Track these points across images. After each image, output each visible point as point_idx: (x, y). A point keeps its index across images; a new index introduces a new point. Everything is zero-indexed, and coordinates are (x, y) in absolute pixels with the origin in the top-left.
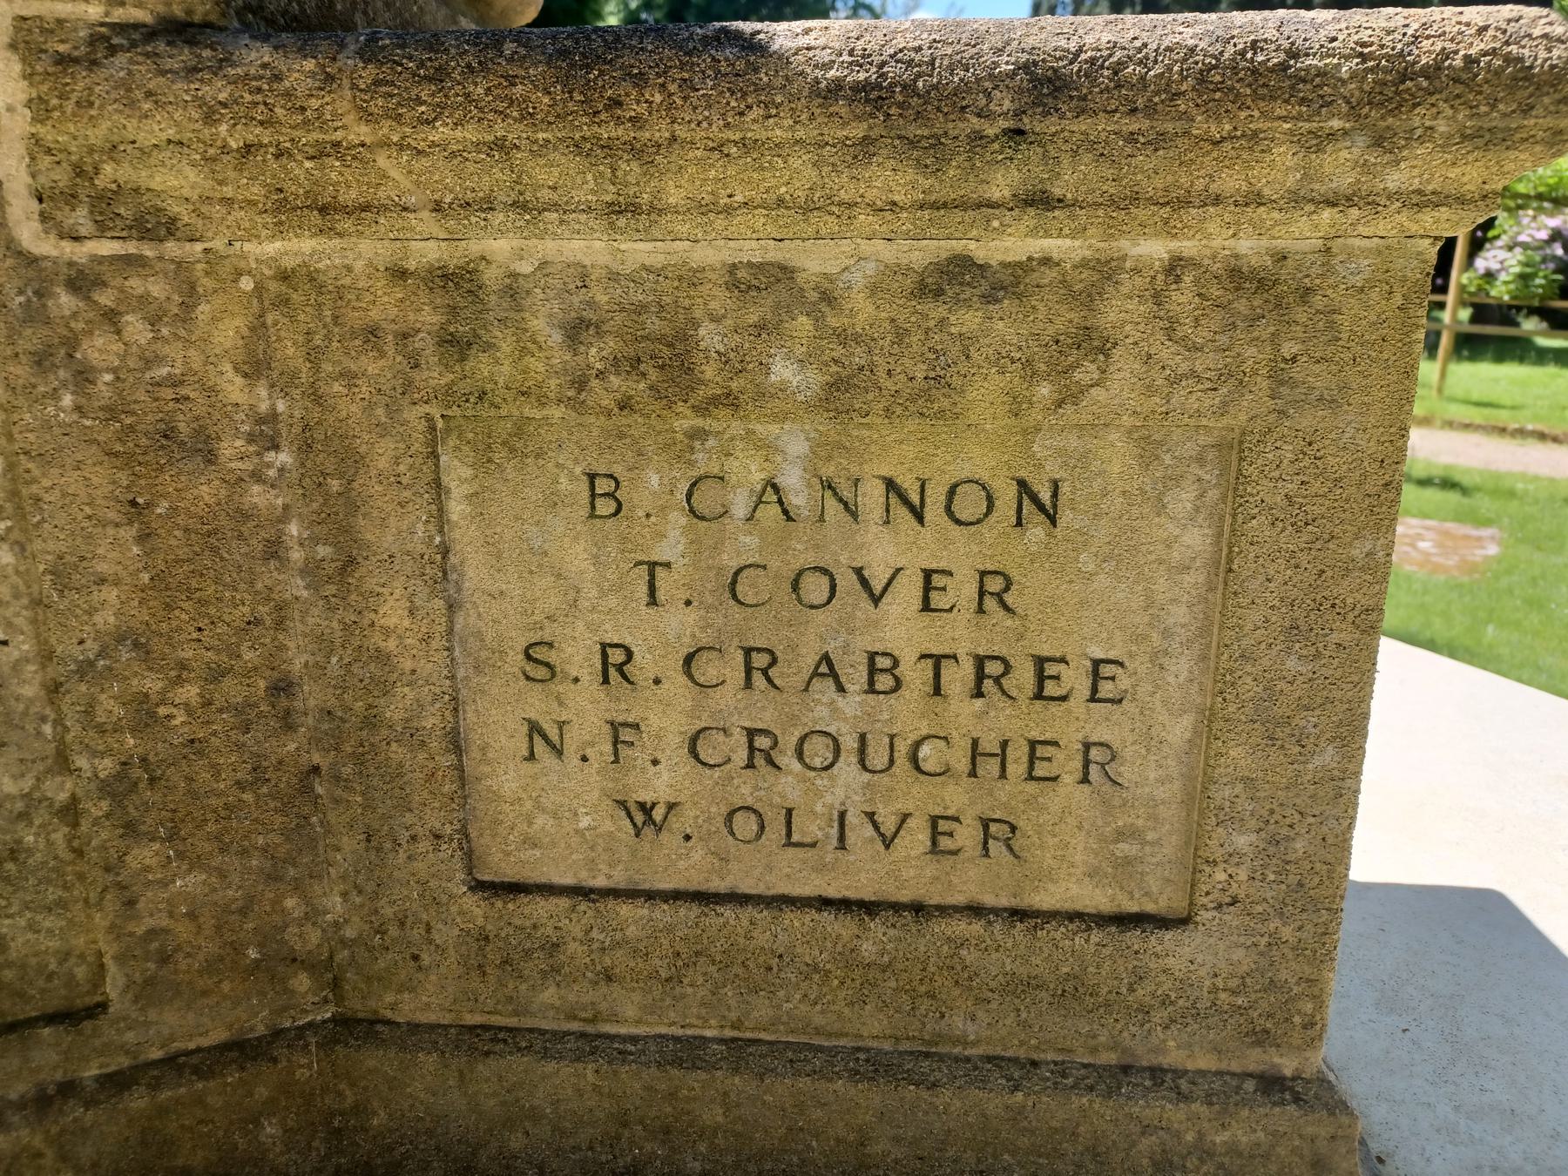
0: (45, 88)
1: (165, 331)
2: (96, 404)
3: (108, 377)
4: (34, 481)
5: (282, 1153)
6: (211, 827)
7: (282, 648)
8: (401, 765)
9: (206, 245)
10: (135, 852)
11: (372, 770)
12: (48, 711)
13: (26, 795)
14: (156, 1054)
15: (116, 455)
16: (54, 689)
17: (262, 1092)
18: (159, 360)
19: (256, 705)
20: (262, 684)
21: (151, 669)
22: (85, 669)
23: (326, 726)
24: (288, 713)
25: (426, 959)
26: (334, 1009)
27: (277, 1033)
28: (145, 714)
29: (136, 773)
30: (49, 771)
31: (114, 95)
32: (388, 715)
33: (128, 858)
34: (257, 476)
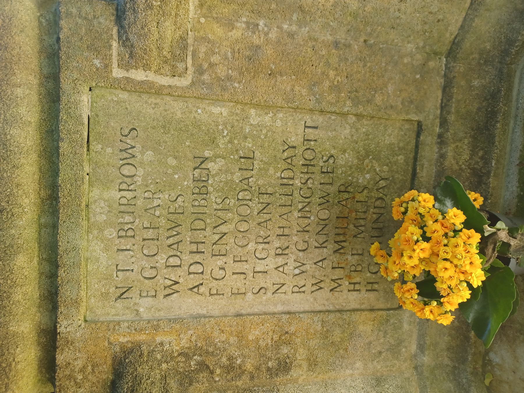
0: (140, 64)
1: (217, 50)
2: (238, 77)
3: (230, 71)
4: (260, 100)
5: (485, 80)
6: (375, 78)
7: (323, 41)
8: (373, 8)
9: (189, 30)
10: (377, 102)
11: (372, 20)
12: (328, 116)
13: (351, 127)
14: (439, 112)
15: (254, 76)
16: (322, 111)
17: (463, 83)
18: (226, 54)
19: (340, 55)
20: (334, 51)
21: (322, 83)
22: (318, 101)
23: (352, 34)
24: (344, 45)
25: (441, 17)
26: (443, 57)
27: (445, 75)
28: (336, 88)
29: (353, 95)
30: (345, 120)
31: (142, 41)
32: (355, 8)
33: (378, 104)
34: (266, 34)
